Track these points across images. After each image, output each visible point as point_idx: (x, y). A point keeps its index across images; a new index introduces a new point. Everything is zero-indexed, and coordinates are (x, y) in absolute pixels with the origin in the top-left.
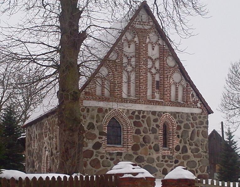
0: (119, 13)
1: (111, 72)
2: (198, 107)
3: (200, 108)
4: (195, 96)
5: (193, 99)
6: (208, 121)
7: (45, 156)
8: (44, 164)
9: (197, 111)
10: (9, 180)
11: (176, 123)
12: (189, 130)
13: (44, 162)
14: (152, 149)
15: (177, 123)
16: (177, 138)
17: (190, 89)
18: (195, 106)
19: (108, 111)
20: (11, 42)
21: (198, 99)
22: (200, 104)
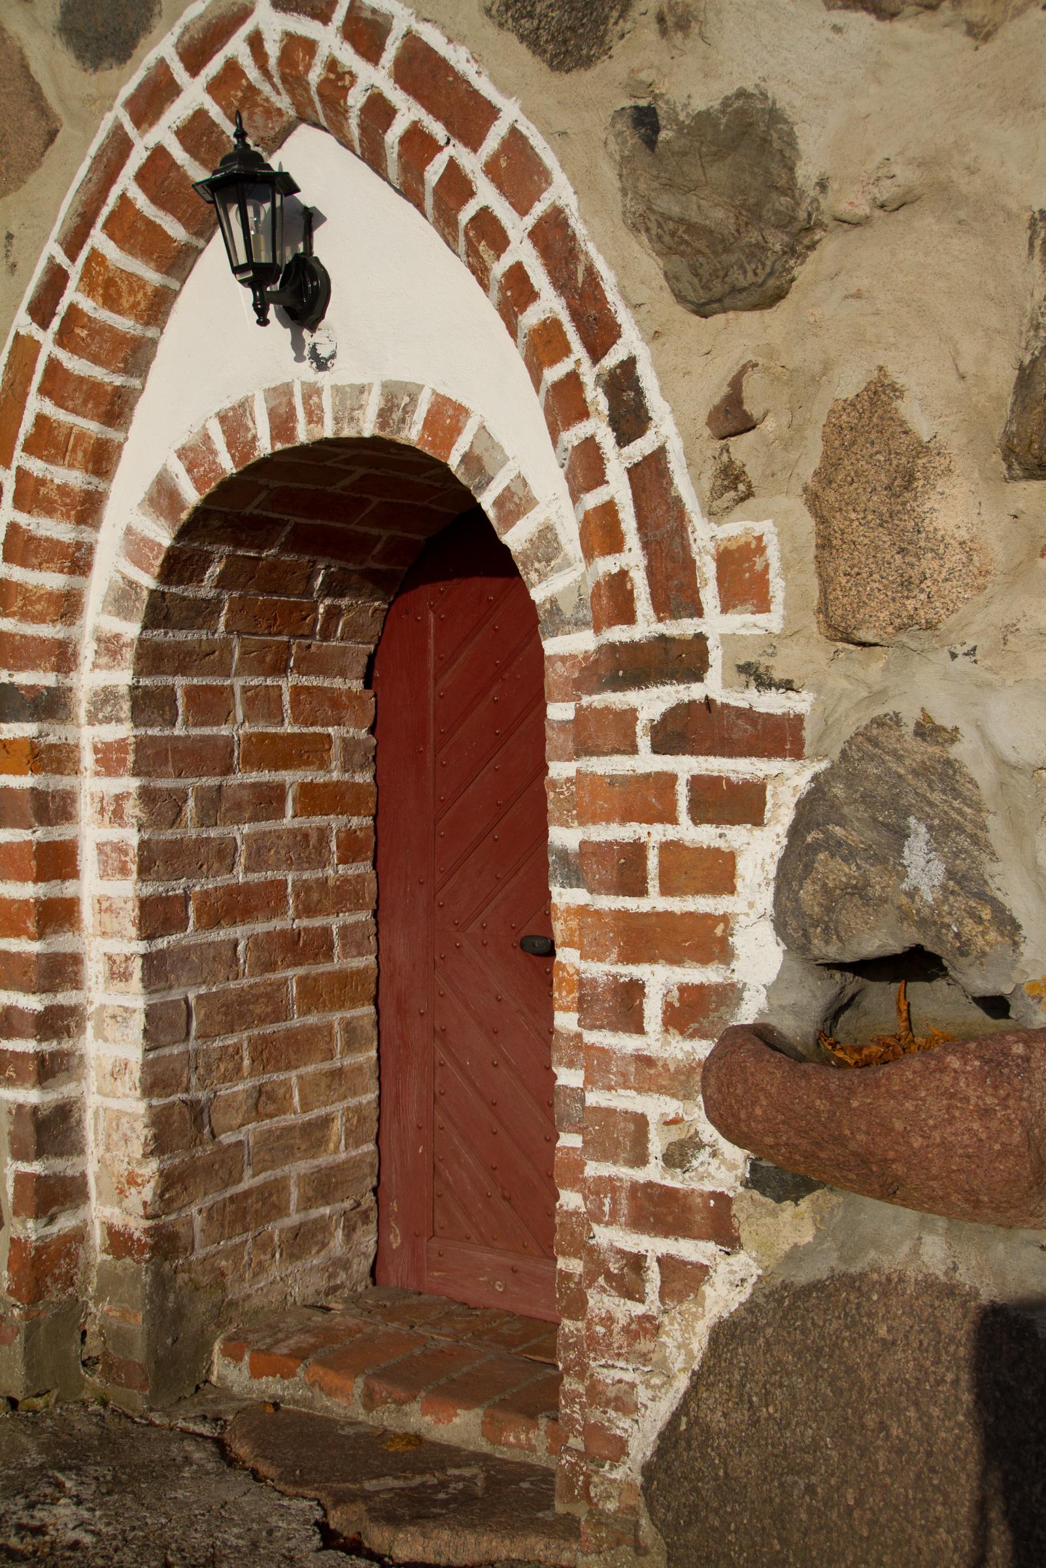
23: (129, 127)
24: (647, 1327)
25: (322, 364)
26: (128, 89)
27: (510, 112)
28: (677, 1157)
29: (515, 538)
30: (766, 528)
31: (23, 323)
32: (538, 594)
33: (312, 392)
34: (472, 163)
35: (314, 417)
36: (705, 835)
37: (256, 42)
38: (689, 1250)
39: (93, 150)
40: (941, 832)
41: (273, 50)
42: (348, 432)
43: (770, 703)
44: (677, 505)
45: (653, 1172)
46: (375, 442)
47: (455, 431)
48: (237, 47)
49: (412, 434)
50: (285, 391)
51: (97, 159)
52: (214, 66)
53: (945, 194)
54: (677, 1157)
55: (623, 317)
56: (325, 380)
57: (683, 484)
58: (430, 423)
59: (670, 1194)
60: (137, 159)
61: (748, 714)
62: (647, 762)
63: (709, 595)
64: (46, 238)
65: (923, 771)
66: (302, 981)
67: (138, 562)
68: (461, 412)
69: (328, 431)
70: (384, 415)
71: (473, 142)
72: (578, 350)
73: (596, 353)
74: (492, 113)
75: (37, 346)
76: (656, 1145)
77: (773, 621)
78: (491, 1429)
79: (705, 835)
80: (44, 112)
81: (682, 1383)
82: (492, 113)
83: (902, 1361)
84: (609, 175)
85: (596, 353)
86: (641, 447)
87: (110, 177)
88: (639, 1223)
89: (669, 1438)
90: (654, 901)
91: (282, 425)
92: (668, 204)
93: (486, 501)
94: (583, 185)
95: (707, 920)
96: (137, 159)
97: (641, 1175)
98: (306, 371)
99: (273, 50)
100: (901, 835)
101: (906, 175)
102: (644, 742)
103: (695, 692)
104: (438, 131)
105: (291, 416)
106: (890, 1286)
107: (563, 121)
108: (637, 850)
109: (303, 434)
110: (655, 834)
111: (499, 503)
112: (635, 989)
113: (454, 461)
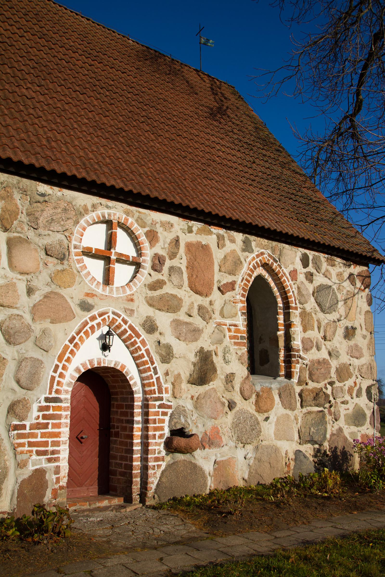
23: (89, 321)
24: (155, 473)
25: (106, 356)
26: (89, 316)
27: (143, 337)
28: (159, 453)
29: (131, 383)
30: (169, 386)
31: (67, 343)
32: (134, 389)
33: (104, 360)
34: (138, 341)
35: (104, 363)
36: (162, 417)
37: (109, 317)
38: (159, 463)
39: (82, 322)
40: (184, 416)
41: (111, 318)
42: (109, 366)
43: (169, 404)
44: (161, 383)
45: (156, 455)
46: (113, 368)
47: (124, 368)
48: (106, 316)
49: (118, 368)
50: (100, 359)
51: (82, 323)
52: (102, 317)
53: (184, 357)
54: (159, 453)
55: (155, 362)
56: (106, 358)
57: (162, 380)
58: (121, 367)
59: (158, 457)
60: (89, 325)
61: (167, 405)
62: (157, 409)
63: (164, 392)
64: (72, 331)
65: (183, 410)
66: (48, 447)
67: (72, 379)
68: (125, 366)
69: (106, 365)
70: (115, 365)
71: (139, 338)
72: (150, 364)
73: (152, 365)
74: (141, 336)
75: (69, 347)
76: (157, 452)
77: (169, 395)
78: (110, 502)
79: (162, 417)
80: (74, 314)
81: (158, 478)
82: (141, 336)
83: (182, 468)
84: (154, 347)
85: (152, 365)
86: (157, 376)
87: (85, 326)
88: (155, 461)
89: (158, 485)
90: (157, 425)
91: (99, 363)
92: (160, 351)
93: (128, 378)
94: (151, 346)
95: (162, 426)
96: (89, 325)
97: (155, 456)
98: (103, 357)
99: (111, 318)
100: (180, 416)
101: (182, 355)
102: (157, 407)
103: (162, 402)
104: (134, 336)
105: (101, 362)
106: (180, 461)
107: (149, 339)
108: (155, 419)
109: (102, 365)
110: (157, 417)
111: (130, 378)
112: (155, 435)
113: (124, 372)
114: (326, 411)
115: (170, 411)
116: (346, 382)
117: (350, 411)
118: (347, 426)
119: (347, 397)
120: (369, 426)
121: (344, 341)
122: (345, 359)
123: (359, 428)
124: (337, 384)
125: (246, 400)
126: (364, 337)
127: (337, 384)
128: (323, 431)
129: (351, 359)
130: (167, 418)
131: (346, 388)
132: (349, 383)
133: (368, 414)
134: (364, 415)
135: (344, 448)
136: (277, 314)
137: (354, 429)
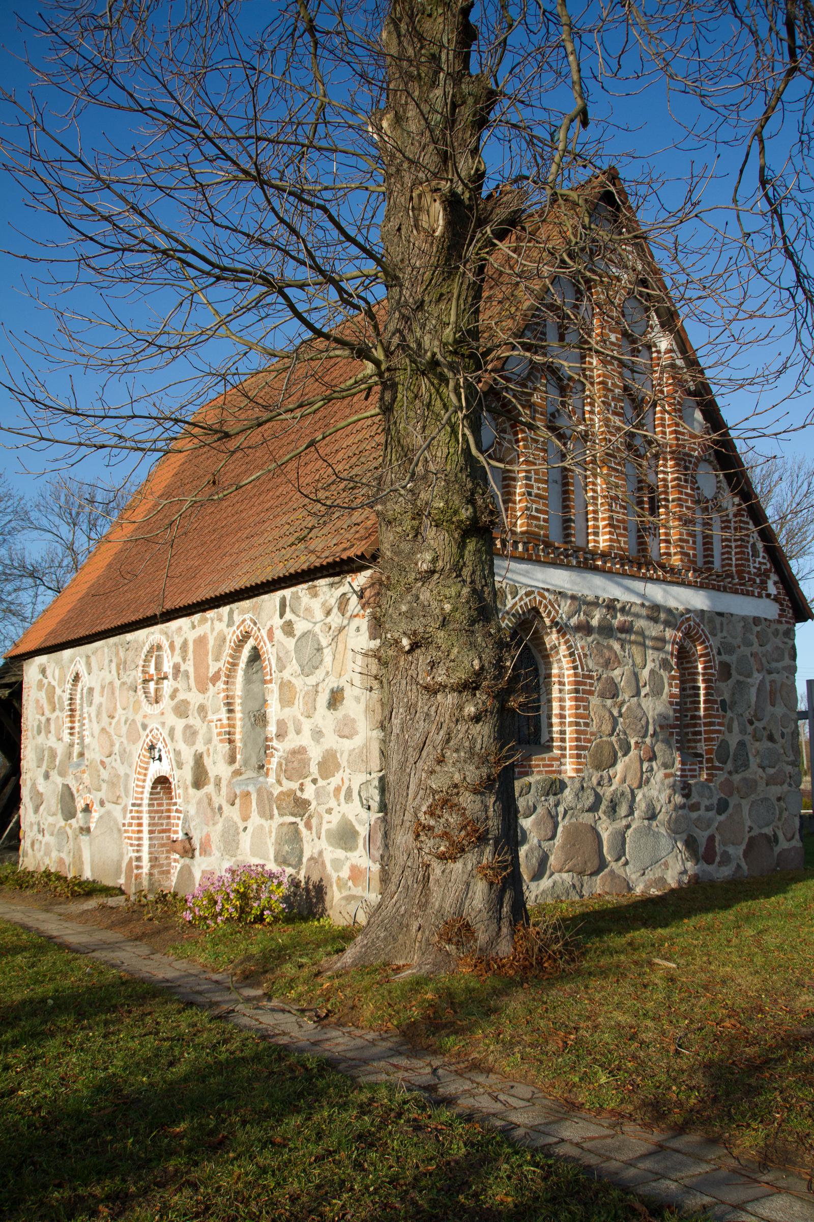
0: (380, 84)
1: (509, 429)
2: (768, 596)
3: (776, 599)
4: (761, 554)
5: (757, 565)
6: (794, 648)
7: (144, 781)
8: (141, 812)
9: (767, 609)
10: (674, 919)
11: (715, 652)
12: (749, 680)
13: (140, 805)
14: (346, 716)
15: (719, 653)
16: (721, 712)
17: (748, 523)
18: (762, 593)
19: (509, 597)
20: (357, 273)
21: (768, 566)
22: (775, 583)
114: (673, 771)
115: (182, 816)
116: (331, 779)
117: (334, 825)
118: (331, 849)
119: (333, 803)
120: (363, 853)
121: (328, 713)
122: (331, 741)
123: (349, 854)
124: (321, 783)
125: (510, 73)
126: (358, 700)
127: (321, 783)
128: (298, 852)
129: (340, 740)
130: (180, 822)
131: (331, 788)
132: (335, 781)
133: (363, 831)
134: (354, 834)
135: (321, 880)
136: (241, 740)
137: (340, 854)
